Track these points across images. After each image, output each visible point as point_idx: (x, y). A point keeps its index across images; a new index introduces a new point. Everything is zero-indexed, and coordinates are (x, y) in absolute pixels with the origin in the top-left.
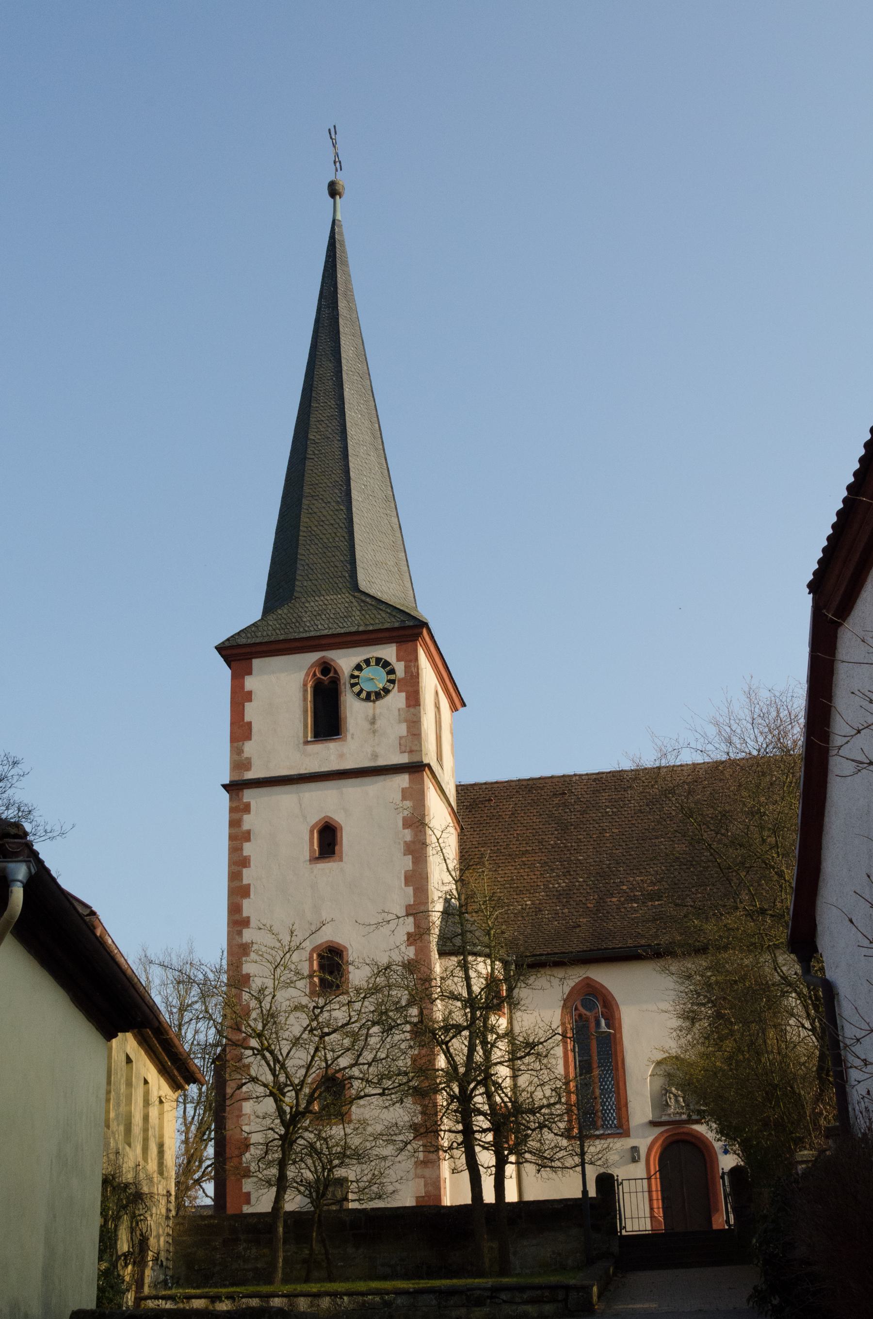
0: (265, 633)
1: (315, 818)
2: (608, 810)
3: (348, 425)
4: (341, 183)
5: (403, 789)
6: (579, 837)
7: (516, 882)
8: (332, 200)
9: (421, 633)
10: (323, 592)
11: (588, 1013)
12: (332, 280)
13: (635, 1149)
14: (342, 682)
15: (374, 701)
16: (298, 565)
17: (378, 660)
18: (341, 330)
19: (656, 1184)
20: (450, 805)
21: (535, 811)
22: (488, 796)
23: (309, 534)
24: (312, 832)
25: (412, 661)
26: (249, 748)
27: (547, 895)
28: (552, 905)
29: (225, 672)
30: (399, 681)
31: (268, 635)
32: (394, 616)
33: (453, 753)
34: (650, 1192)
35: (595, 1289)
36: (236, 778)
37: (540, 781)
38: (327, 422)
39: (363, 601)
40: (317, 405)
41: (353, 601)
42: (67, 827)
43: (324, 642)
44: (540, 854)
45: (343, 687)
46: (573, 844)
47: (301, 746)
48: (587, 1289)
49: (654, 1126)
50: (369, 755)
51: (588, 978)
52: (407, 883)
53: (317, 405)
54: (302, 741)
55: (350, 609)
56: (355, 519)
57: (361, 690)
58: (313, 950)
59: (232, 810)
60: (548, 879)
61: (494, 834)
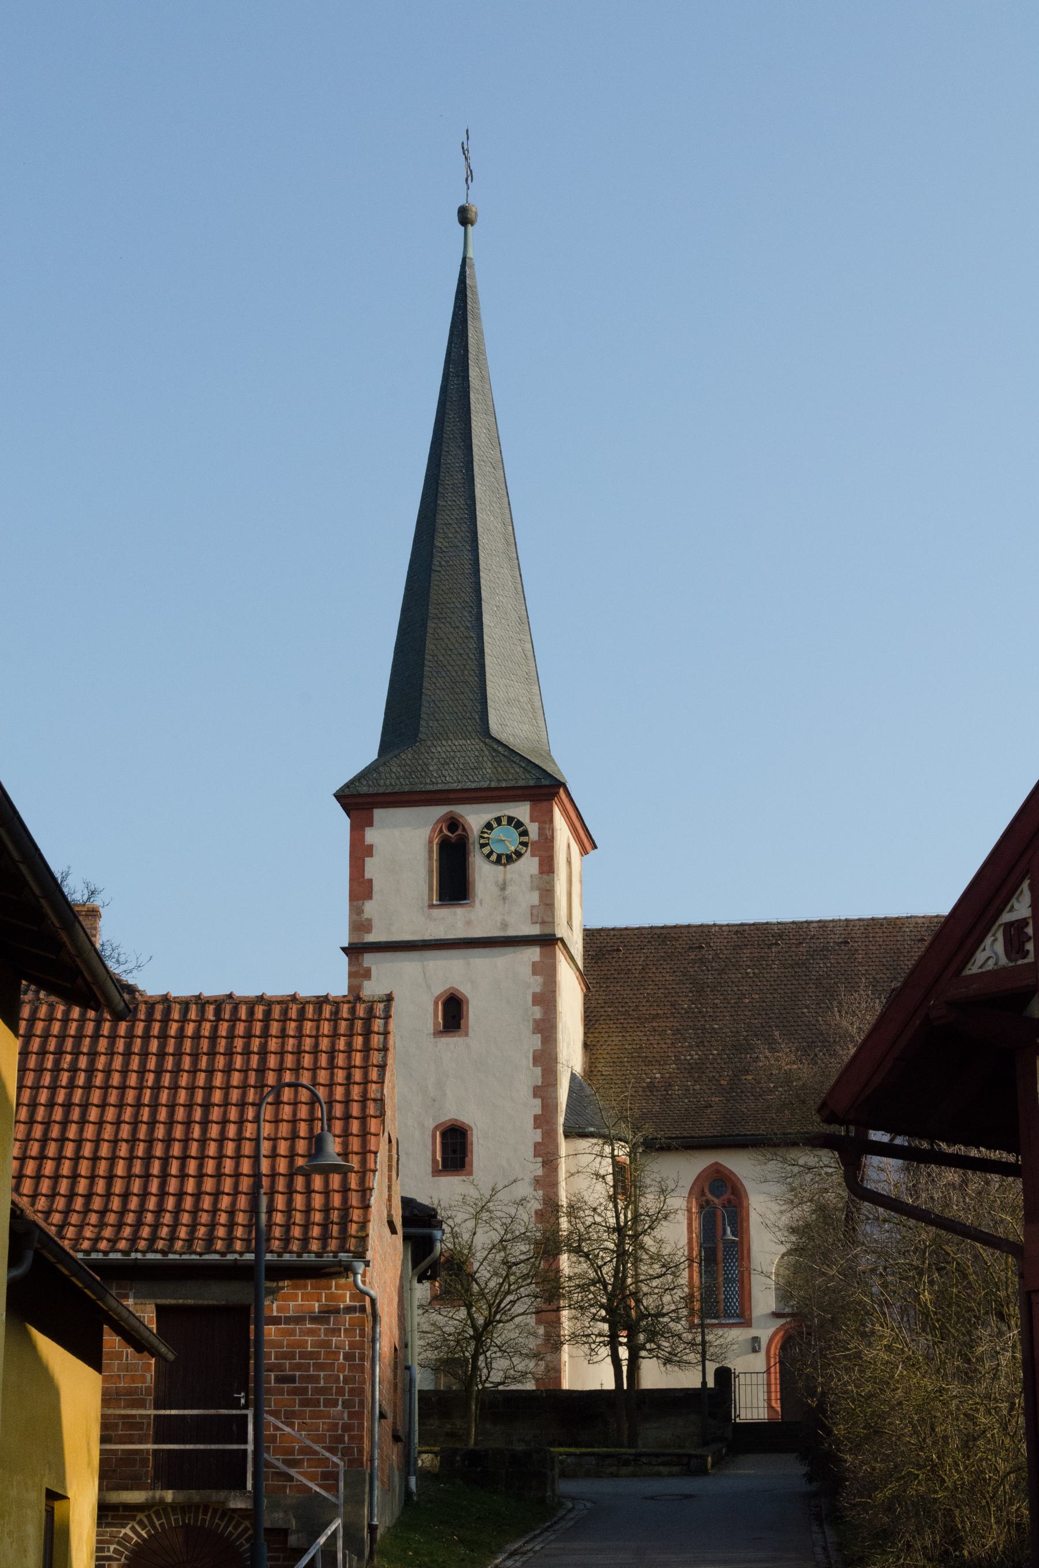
0: (388, 782)
1: (439, 989)
2: (749, 970)
3: (480, 530)
4: (474, 209)
5: (533, 962)
6: (715, 1001)
7: (644, 1050)
8: (463, 228)
9: (558, 793)
10: (451, 736)
11: (716, 1201)
12: (462, 340)
13: (756, 1340)
14: (471, 841)
15: (505, 865)
16: (424, 703)
17: (510, 820)
18: (472, 408)
19: (775, 1378)
20: (578, 969)
21: (669, 966)
22: (616, 945)
23: (435, 664)
24: (436, 1004)
25: (546, 822)
26: (370, 908)
27: (678, 1069)
28: (684, 1079)
29: (343, 822)
30: (532, 845)
31: (391, 785)
32: (529, 772)
33: (581, 906)
34: (769, 1384)
35: (710, 1459)
36: (356, 941)
37: (675, 930)
38: (455, 526)
39: (495, 750)
40: (444, 503)
41: (484, 749)
42: (143, 959)
43: (451, 796)
44: (672, 1019)
45: (471, 847)
46: (709, 1010)
47: (426, 909)
48: (704, 1458)
50: (499, 924)
51: (717, 1163)
52: (535, 1064)
53: (444, 503)
54: (426, 904)
55: (481, 759)
56: (487, 650)
57: (492, 852)
58: (436, 1128)
59: (351, 975)
60: (680, 1050)
61: (622, 993)
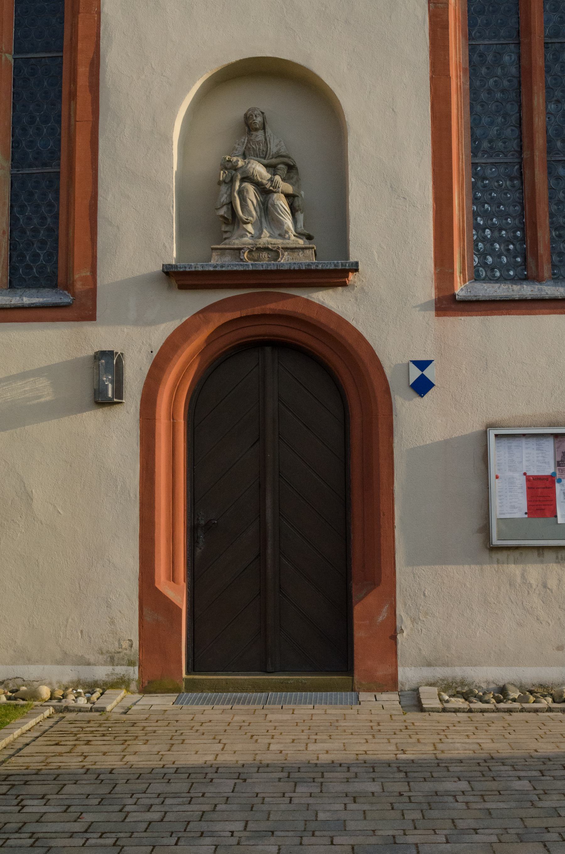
49: (182, 287)
